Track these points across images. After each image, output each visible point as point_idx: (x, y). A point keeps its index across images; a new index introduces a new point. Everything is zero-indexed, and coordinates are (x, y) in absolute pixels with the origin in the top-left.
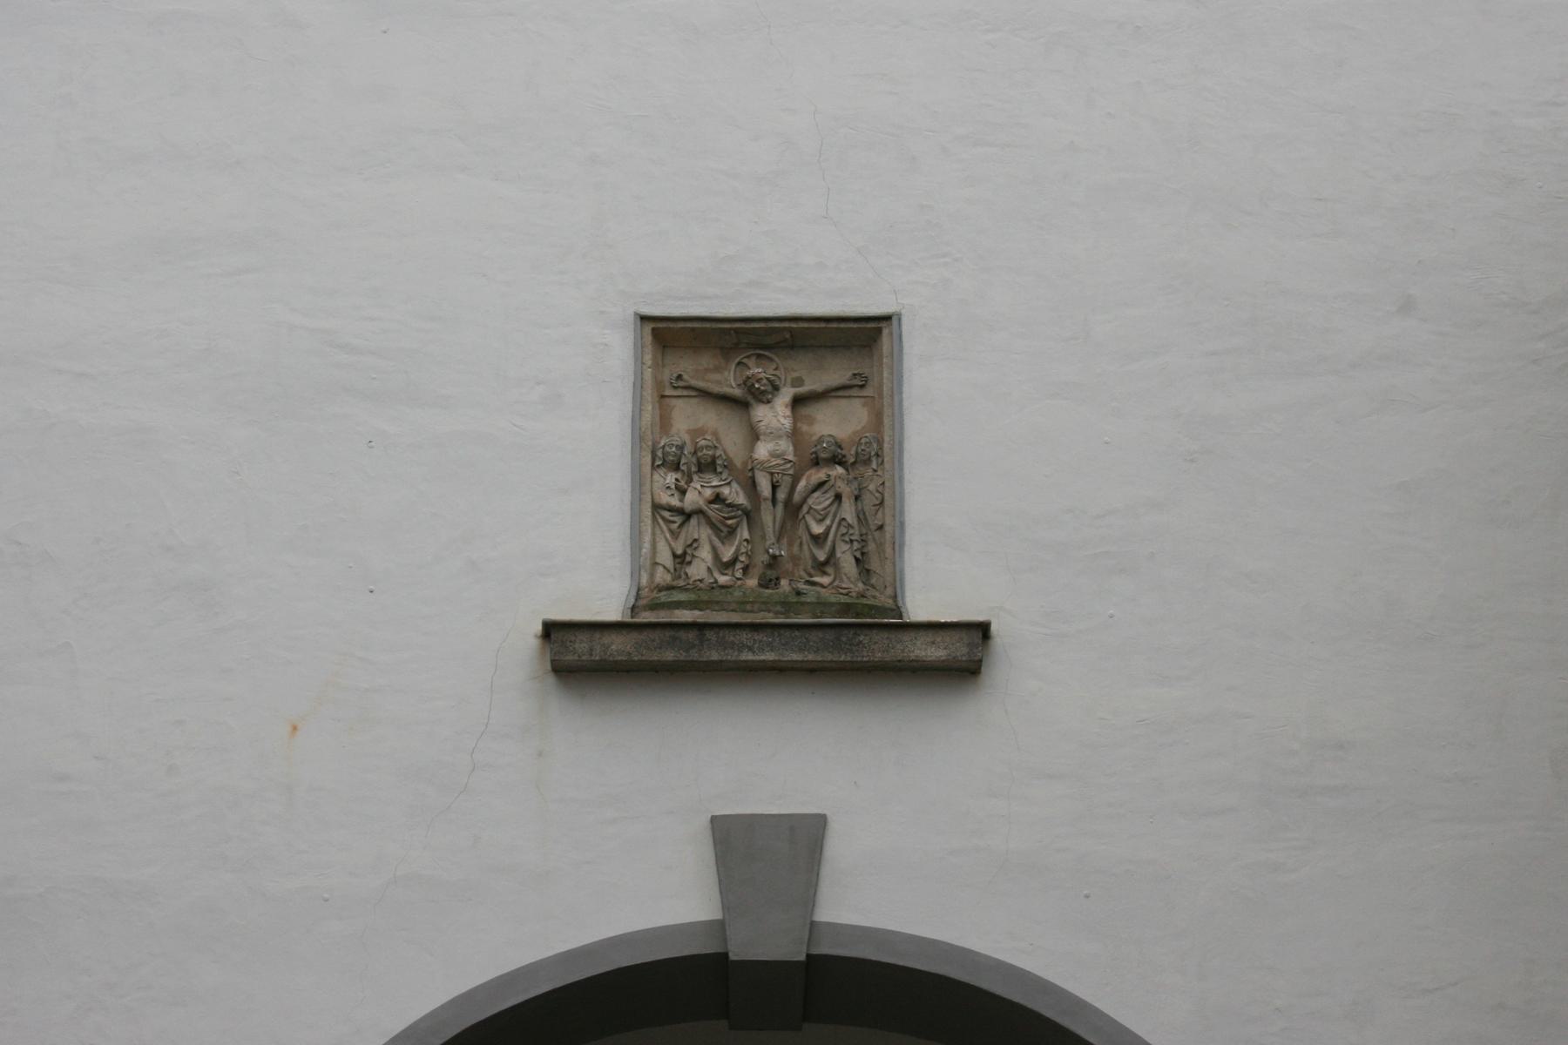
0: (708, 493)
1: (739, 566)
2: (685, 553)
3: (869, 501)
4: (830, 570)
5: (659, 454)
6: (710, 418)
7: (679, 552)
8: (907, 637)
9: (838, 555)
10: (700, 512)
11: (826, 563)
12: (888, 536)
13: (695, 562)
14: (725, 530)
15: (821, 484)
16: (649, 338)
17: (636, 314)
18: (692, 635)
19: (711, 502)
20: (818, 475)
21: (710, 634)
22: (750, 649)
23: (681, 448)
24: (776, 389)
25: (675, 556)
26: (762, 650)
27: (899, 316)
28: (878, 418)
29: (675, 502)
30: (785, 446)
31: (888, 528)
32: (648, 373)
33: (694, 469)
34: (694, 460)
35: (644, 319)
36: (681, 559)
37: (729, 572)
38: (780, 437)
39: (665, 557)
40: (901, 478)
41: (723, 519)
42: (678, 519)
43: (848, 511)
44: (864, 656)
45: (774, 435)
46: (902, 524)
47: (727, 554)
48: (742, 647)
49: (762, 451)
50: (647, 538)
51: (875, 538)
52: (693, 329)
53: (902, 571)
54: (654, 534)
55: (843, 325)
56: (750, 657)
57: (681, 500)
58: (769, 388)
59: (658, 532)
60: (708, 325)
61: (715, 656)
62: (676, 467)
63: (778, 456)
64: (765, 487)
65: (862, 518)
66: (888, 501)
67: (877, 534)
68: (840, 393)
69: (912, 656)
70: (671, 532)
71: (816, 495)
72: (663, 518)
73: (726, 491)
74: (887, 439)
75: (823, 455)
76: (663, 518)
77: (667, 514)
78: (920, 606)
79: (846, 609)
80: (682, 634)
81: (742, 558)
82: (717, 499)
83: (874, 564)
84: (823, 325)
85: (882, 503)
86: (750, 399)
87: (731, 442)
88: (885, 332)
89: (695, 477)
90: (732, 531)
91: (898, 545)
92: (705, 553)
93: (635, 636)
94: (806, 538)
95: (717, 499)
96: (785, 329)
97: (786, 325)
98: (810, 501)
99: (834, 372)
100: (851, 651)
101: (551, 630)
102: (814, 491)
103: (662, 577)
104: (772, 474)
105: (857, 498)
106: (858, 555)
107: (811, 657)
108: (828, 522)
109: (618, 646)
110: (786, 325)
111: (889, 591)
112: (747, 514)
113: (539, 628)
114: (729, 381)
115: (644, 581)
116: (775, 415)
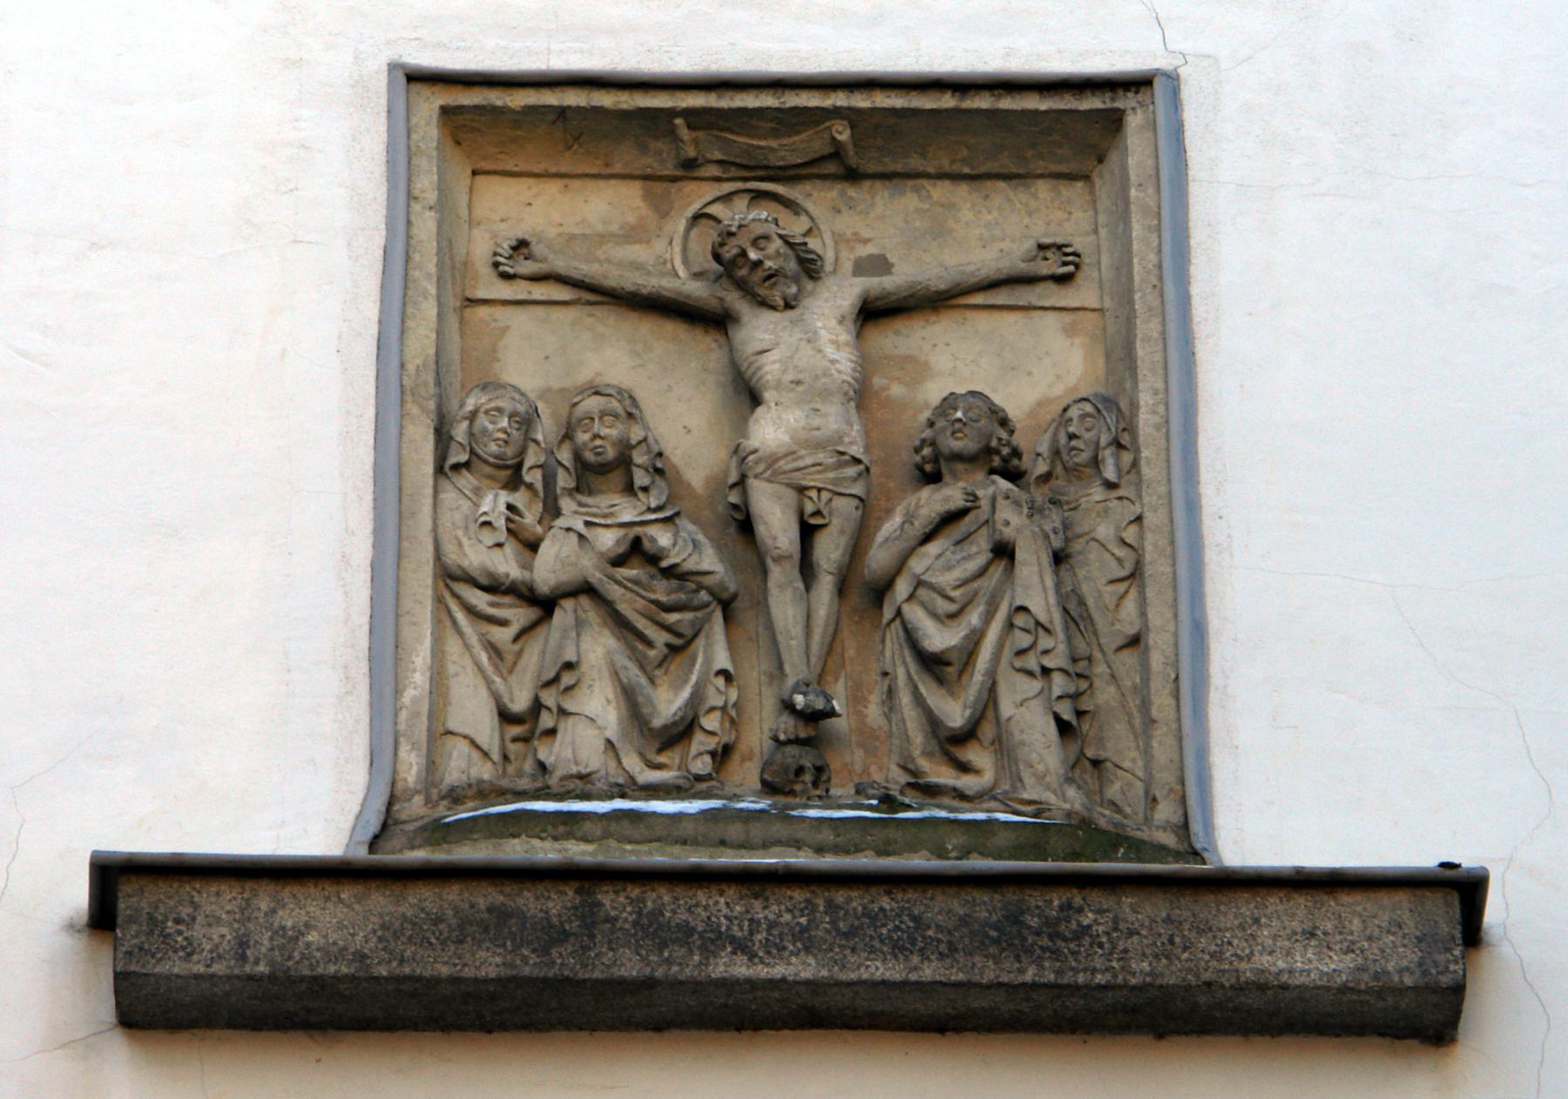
0: (607, 540)
1: (700, 743)
2: (537, 707)
3: (1096, 573)
4: (975, 755)
5: (460, 432)
6: (615, 355)
7: (520, 704)
8: (1232, 912)
9: (1006, 708)
10: (586, 589)
11: (967, 735)
12: (1156, 660)
13: (567, 728)
14: (660, 638)
15: (950, 518)
16: (428, 129)
17: (393, 67)
18: (557, 903)
19: (619, 561)
20: (933, 501)
21: (610, 900)
22: (742, 947)
23: (526, 421)
24: (810, 268)
25: (506, 717)
26: (775, 948)
27: (1173, 79)
28: (1121, 356)
29: (507, 564)
30: (835, 419)
31: (1159, 642)
32: (426, 225)
33: (564, 480)
34: (565, 455)
35: (417, 78)
36: (525, 724)
37: (671, 757)
38: (825, 394)
39: (473, 712)
40: (1193, 506)
41: (664, 605)
42: (519, 615)
43: (1034, 586)
44: (1094, 969)
45: (807, 389)
46: (1199, 630)
47: (668, 704)
48: (714, 940)
49: (770, 430)
50: (421, 658)
51: (1127, 656)
52: (562, 112)
53: (1203, 753)
54: (438, 653)
55: (1007, 103)
56: (741, 969)
57: (527, 566)
58: (792, 266)
59: (453, 646)
60: (605, 99)
61: (630, 966)
62: (513, 478)
63: (819, 446)
64: (776, 521)
65: (1076, 615)
66: (1156, 567)
67: (1129, 658)
68: (1000, 297)
69: (1247, 971)
70: (494, 650)
71: (933, 548)
72: (470, 610)
73: (662, 538)
74: (1145, 399)
75: (957, 445)
76: (470, 610)
77: (480, 599)
78: (1261, 819)
79: (1035, 838)
80: (529, 901)
81: (711, 722)
82: (636, 551)
83: (1119, 744)
84: (948, 101)
85: (1136, 575)
86: (734, 300)
87: (679, 412)
88: (1134, 121)
89: (567, 504)
90: (680, 647)
91: (1190, 683)
92: (598, 705)
93: (380, 903)
94: (904, 669)
95: (636, 551)
96: (836, 112)
97: (839, 99)
98: (917, 565)
99: (986, 228)
100: (1056, 954)
101: (113, 878)
102: (927, 538)
103: (460, 766)
104: (801, 490)
105: (1059, 558)
106: (1067, 715)
107: (929, 971)
108: (974, 618)
109: (328, 929)
110: (839, 99)
111: (1166, 812)
112: (727, 606)
113: (77, 895)
114: (669, 258)
115: (411, 766)
116: (802, 345)
